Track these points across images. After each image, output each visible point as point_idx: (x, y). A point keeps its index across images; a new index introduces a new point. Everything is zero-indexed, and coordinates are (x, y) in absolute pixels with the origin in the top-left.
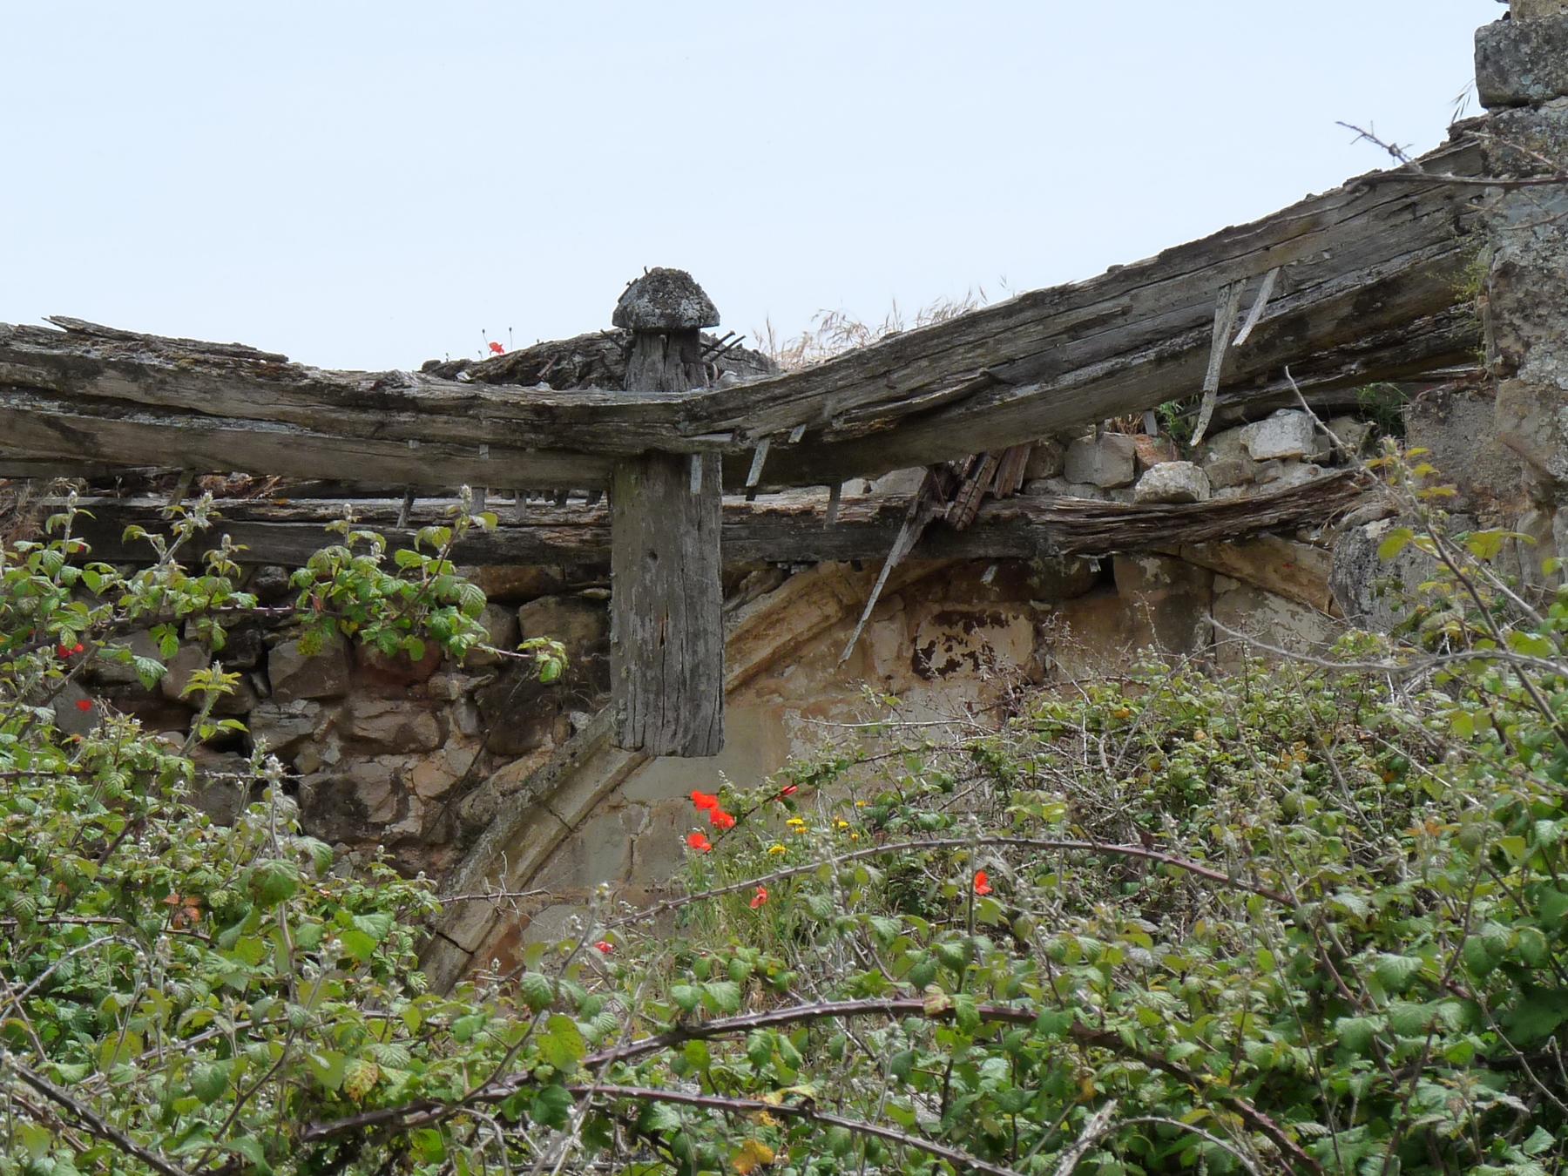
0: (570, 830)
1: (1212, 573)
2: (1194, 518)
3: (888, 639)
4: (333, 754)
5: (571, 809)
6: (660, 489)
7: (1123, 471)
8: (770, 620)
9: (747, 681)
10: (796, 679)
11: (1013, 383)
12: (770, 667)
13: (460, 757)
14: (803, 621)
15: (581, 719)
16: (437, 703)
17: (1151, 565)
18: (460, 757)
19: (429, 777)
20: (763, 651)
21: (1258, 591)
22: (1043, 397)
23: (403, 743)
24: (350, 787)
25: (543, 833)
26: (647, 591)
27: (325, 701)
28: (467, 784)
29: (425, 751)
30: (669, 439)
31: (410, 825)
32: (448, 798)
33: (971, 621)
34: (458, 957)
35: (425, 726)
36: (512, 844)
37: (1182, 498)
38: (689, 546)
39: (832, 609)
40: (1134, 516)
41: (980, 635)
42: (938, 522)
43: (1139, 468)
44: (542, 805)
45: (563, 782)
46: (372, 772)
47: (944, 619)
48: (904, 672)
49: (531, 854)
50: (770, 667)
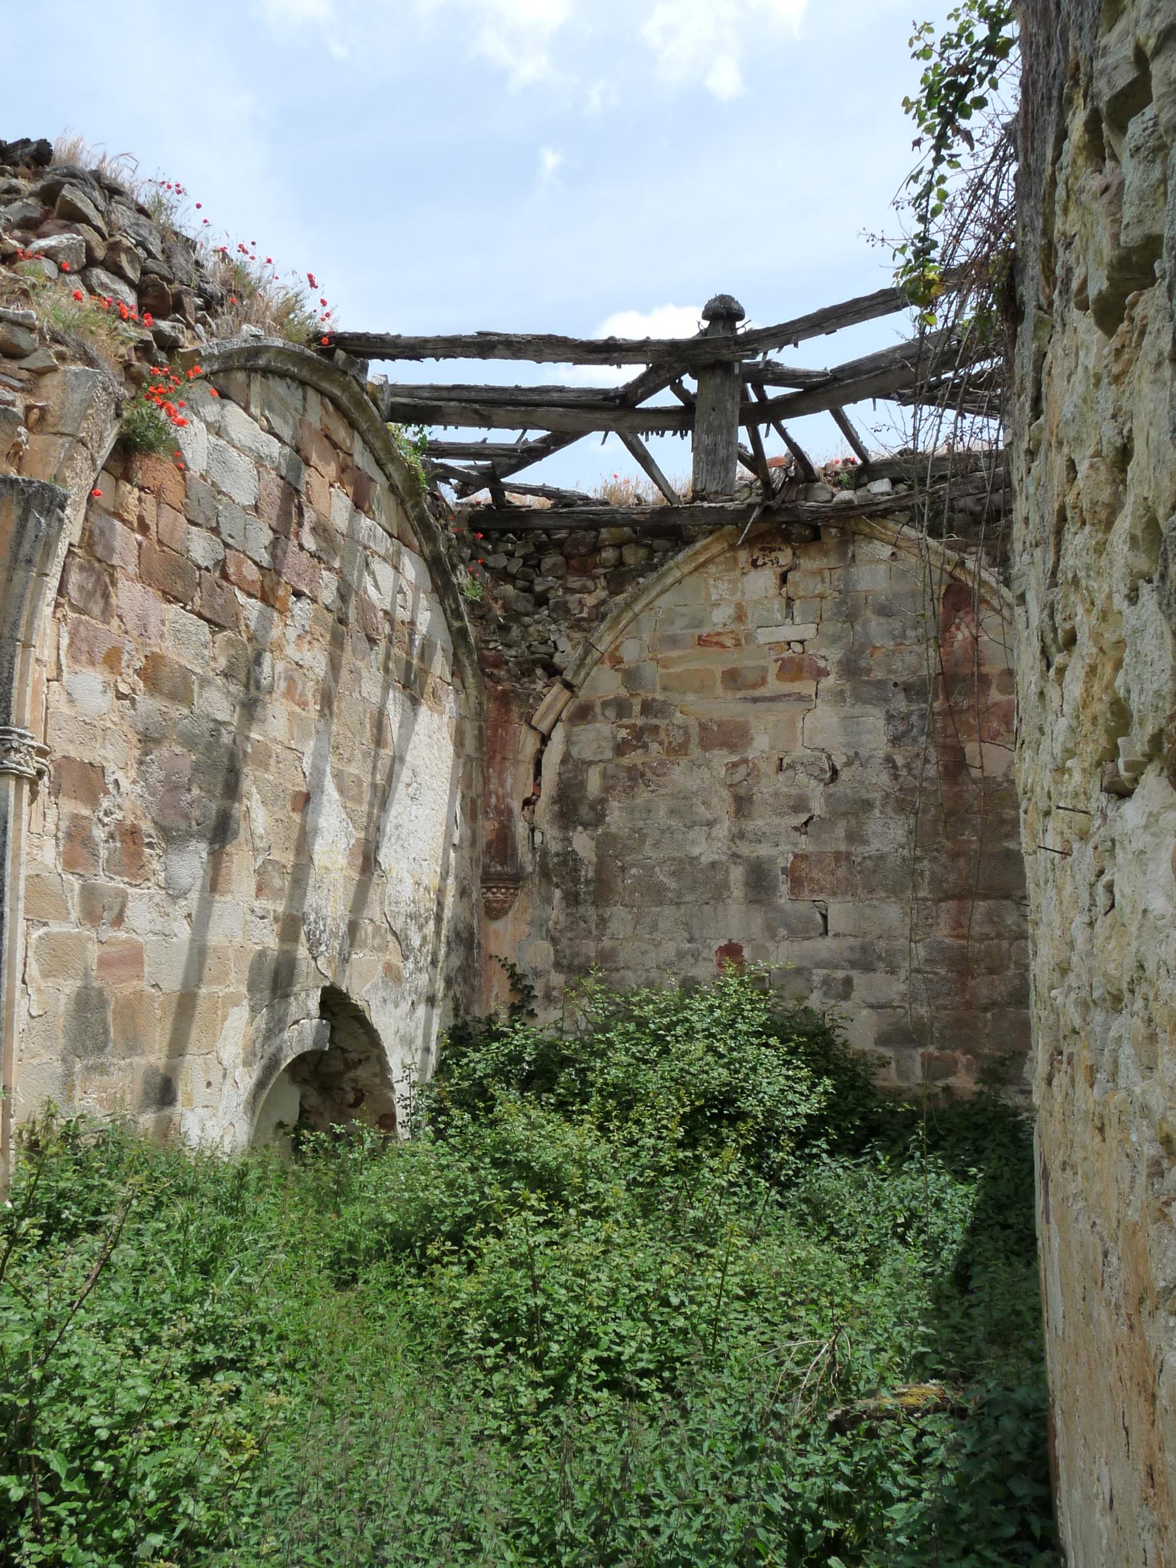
0: (636, 615)
1: (854, 533)
2: (854, 508)
3: (743, 556)
4: (560, 593)
5: (637, 608)
6: (719, 381)
7: (827, 497)
8: (705, 548)
9: (696, 569)
10: (712, 569)
11: (842, 380)
12: (704, 565)
13: (602, 594)
14: (716, 549)
15: (641, 580)
16: (594, 578)
17: (834, 531)
18: (602, 594)
19: (590, 600)
20: (702, 559)
21: (870, 538)
22: (854, 383)
23: (584, 590)
24: (566, 603)
25: (628, 615)
26: (710, 424)
27: (558, 578)
28: (603, 602)
29: (590, 592)
30: (726, 355)
31: (584, 615)
32: (596, 607)
33: (772, 550)
34: (598, 654)
35: (590, 584)
36: (617, 620)
37: (850, 502)
38: (729, 406)
39: (725, 545)
40: (833, 509)
41: (774, 554)
42: (768, 507)
43: (833, 495)
44: (628, 605)
45: (635, 599)
46: (573, 599)
47: (763, 549)
48: (748, 567)
49: (624, 622)
50: (704, 565)
